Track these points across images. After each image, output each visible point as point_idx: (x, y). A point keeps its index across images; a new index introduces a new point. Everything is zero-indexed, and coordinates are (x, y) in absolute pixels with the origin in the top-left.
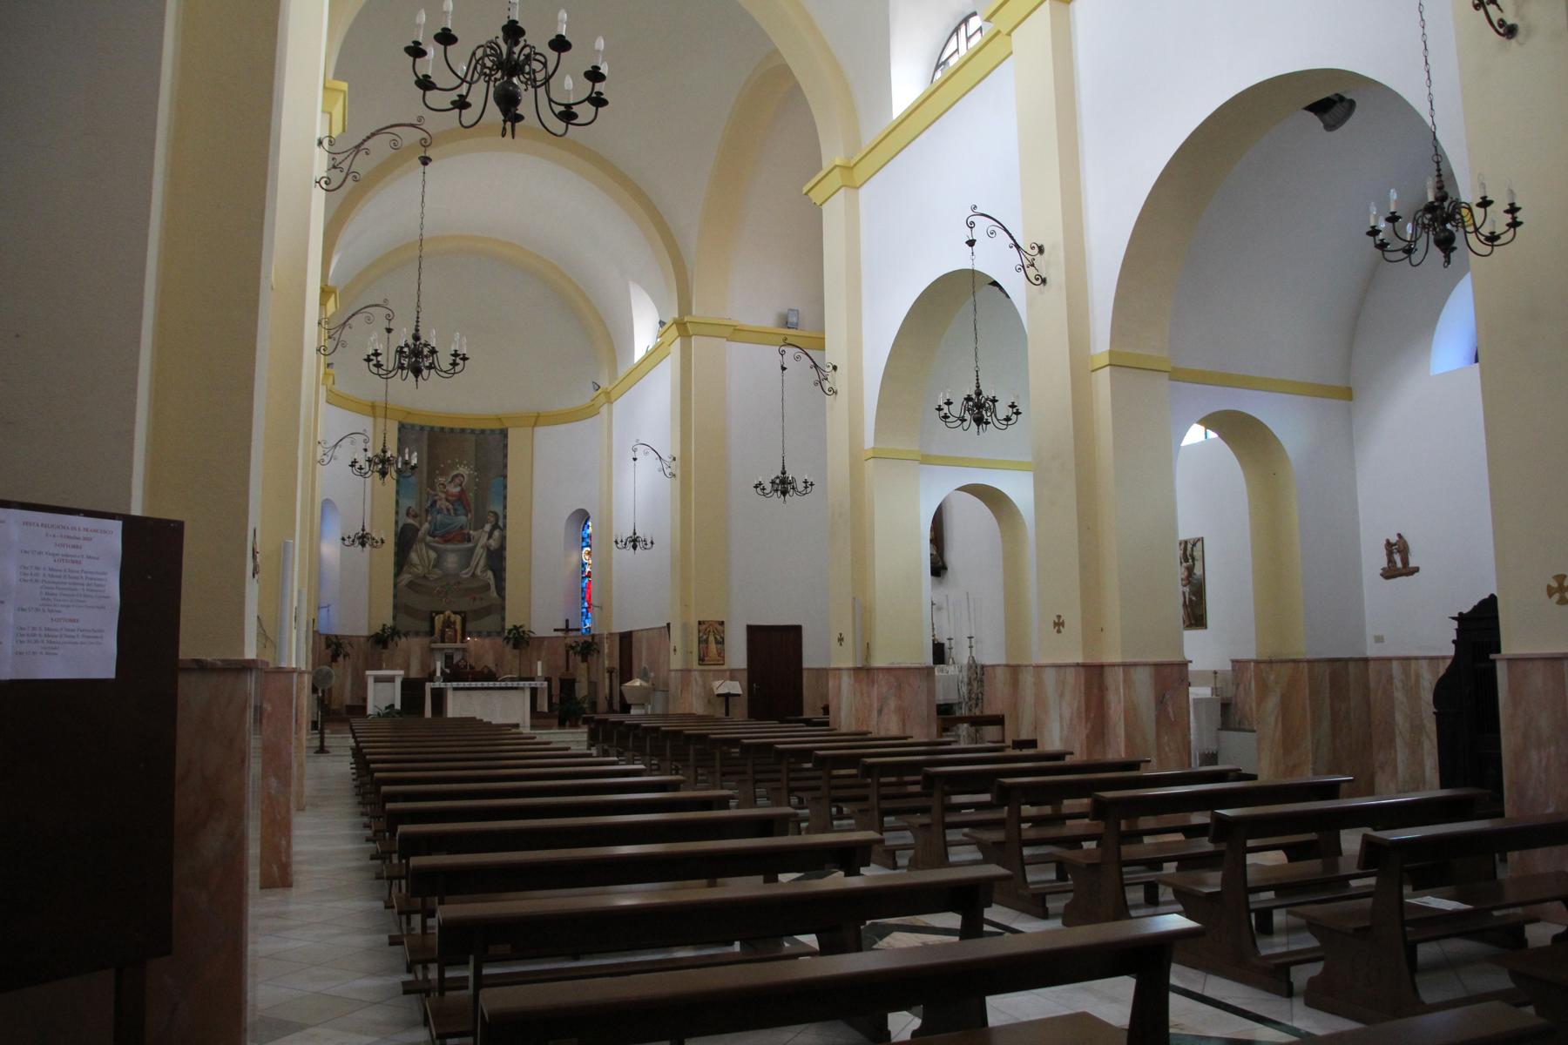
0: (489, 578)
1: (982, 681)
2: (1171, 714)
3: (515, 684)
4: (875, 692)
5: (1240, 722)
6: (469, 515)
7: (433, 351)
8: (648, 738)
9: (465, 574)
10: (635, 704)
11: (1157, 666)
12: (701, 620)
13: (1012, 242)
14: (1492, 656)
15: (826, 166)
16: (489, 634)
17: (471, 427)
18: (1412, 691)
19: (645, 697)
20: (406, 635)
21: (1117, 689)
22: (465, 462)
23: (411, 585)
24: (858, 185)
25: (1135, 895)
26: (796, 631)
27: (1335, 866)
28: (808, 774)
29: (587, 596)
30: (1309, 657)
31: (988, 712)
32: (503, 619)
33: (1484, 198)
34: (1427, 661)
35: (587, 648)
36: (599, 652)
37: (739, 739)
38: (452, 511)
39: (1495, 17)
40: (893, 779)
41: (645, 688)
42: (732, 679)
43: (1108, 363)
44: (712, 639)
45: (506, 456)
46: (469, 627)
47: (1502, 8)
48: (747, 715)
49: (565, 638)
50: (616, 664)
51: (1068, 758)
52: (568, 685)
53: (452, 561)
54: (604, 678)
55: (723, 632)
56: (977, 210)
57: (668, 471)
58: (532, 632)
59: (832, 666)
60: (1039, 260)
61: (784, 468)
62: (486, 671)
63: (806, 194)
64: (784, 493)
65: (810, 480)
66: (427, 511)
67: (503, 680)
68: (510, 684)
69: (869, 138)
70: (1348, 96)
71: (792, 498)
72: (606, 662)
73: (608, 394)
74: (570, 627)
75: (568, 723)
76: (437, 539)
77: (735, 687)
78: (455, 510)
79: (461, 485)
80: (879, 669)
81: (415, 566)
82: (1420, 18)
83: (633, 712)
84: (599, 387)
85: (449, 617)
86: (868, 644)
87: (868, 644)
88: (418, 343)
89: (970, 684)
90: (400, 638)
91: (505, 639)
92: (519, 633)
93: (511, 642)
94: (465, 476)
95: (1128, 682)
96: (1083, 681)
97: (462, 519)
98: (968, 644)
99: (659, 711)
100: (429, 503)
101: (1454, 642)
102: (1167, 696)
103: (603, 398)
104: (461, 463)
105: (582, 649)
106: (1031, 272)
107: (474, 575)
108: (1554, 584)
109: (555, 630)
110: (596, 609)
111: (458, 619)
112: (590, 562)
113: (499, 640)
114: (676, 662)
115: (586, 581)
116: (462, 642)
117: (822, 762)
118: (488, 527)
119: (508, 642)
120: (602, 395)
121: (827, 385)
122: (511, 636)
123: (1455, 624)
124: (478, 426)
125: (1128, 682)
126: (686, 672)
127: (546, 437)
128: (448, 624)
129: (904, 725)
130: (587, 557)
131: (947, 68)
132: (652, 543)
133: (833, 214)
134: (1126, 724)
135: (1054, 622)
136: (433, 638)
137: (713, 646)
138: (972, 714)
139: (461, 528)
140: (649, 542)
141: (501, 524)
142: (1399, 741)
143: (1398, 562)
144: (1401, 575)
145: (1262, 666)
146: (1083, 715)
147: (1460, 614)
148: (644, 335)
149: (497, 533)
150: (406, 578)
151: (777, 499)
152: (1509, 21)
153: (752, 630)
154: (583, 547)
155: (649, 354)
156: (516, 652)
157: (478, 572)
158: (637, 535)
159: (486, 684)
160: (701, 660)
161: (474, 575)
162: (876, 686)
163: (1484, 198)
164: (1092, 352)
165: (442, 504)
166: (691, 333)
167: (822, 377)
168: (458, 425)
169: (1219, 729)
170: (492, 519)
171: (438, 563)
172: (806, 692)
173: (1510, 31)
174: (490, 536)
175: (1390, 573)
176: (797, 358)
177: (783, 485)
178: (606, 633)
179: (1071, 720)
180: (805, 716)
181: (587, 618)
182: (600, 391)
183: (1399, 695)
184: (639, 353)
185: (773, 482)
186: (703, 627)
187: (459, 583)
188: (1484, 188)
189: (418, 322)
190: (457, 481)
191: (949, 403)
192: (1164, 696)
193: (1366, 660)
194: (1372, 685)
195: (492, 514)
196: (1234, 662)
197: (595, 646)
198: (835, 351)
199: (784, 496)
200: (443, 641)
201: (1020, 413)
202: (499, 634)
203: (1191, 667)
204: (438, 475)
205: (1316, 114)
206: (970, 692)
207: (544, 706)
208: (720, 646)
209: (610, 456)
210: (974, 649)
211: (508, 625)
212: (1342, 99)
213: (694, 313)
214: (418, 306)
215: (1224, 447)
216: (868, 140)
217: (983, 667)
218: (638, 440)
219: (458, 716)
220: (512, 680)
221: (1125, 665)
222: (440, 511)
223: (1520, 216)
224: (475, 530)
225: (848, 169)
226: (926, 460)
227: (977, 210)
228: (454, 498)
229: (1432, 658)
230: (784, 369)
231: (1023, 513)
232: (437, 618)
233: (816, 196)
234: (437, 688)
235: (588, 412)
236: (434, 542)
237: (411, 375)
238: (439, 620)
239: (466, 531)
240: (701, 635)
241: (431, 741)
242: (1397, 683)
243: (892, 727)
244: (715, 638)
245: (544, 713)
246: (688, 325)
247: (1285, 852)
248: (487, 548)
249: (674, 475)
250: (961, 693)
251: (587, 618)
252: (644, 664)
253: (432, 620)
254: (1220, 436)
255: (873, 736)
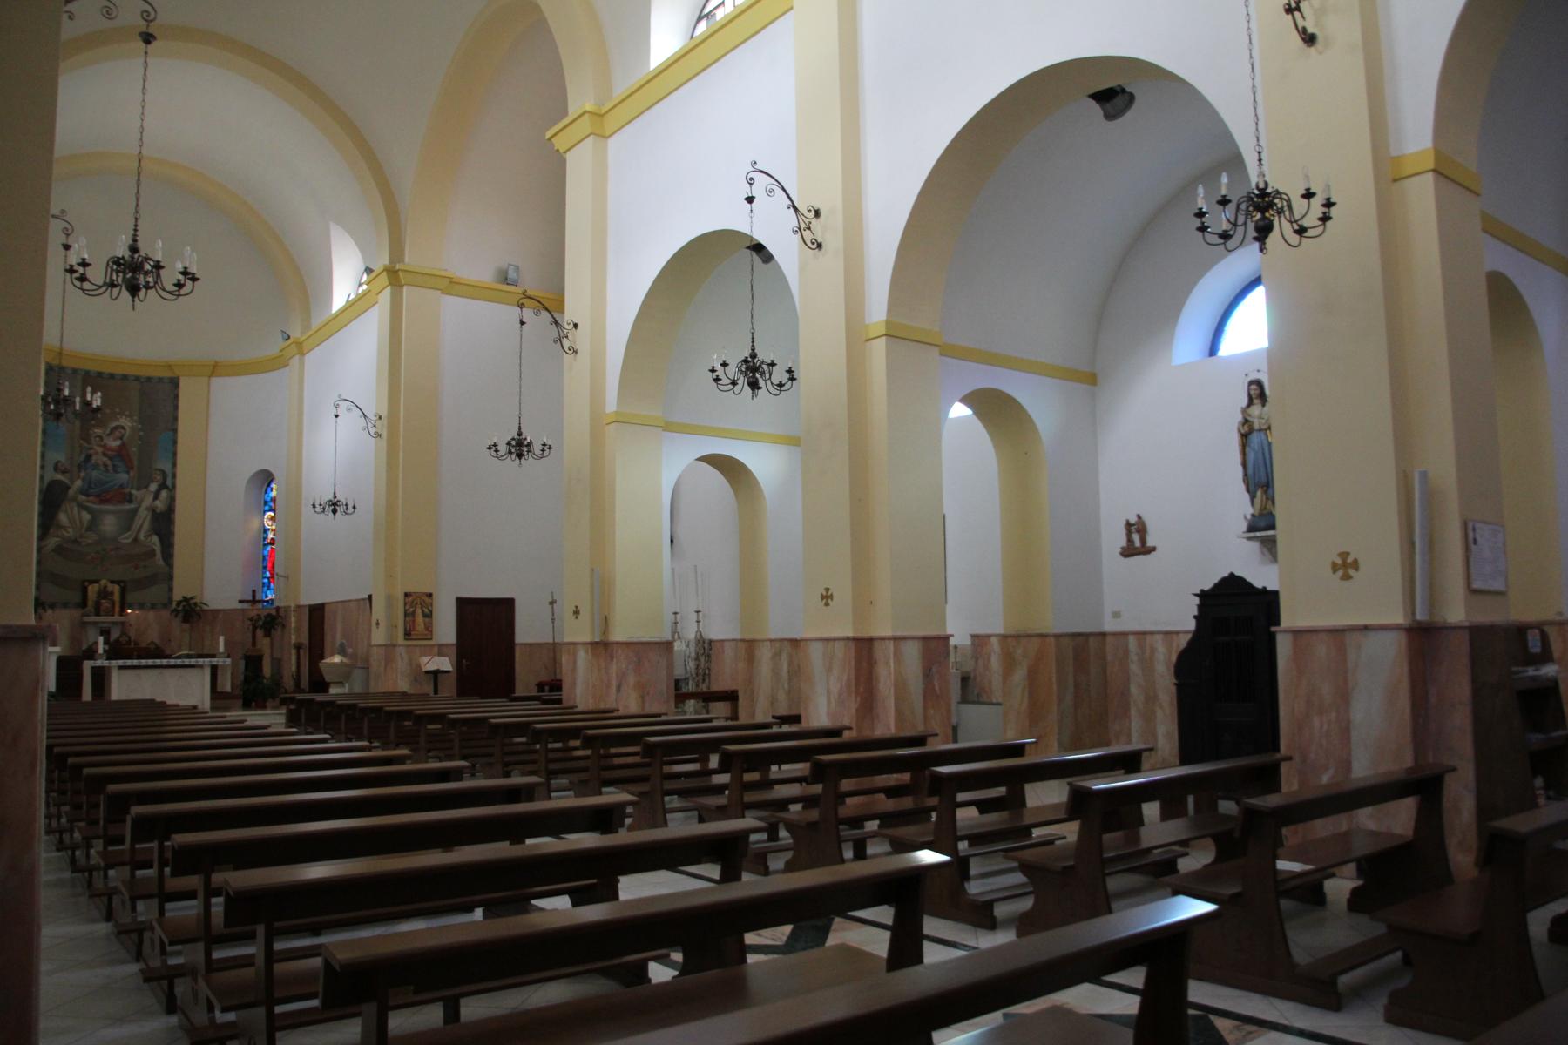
0: (154, 544)
1: (709, 656)
2: (937, 688)
3: (193, 661)
4: (614, 669)
5: (978, 695)
6: (132, 473)
7: (158, 266)
8: (366, 719)
9: (126, 539)
10: (334, 683)
11: (925, 639)
12: (408, 590)
13: (790, 203)
14: (1273, 629)
15: (573, 110)
16: (153, 606)
17: (148, 374)
18: (1147, 664)
19: (345, 674)
20: (53, 606)
21: (887, 663)
22: (127, 413)
23: (59, 550)
24: (608, 134)
25: (848, 854)
26: (508, 604)
27: (1136, 839)
28: (521, 748)
29: (269, 565)
30: (1056, 631)
31: (715, 687)
32: (171, 590)
33: (1308, 190)
34: (1161, 635)
35: (271, 622)
36: (284, 626)
37: (486, 719)
38: (110, 468)
39: (1301, 23)
40: (558, 745)
41: (346, 665)
42: (440, 654)
43: (884, 332)
44: (419, 611)
45: (176, 407)
46: (130, 598)
47: (1305, 15)
48: (455, 691)
49: (253, 610)
50: (305, 639)
51: (846, 734)
52: (253, 662)
53: (109, 524)
54: (291, 654)
55: (431, 605)
56: (756, 167)
57: (372, 431)
58: (206, 605)
59: (567, 639)
60: (815, 223)
61: (520, 429)
62: (152, 647)
63: (550, 139)
64: (520, 456)
65: (548, 443)
66: (79, 467)
67: (177, 658)
68: (187, 662)
69: (620, 88)
70: (1129, 89)
71: (528, 461)
72: (293, 637)
73: (299, 344)
74: (251, 598)
75: (253, 704)
76: (91, 498)
77: (445, 664)
78: (114, 466)
79: (121, 438)
80: (618, 643)
81: (64, 528)
82: (1245, 12)
83: (333, 690)
84: (289, 337)
85: (105, 587)
86: (606, 617)
87: (606, 617)
88: (136, 256)
89: (697, 659)
90: (45, 611)
91: (173, 611)
92: (189, 605)
93: (181, 615)
94: (128, 430)
95: (898, 654)
96: (853, 655)
97: (123, 477)
98: (695, 619)
99: (358, 689)
100: (83, 457)
101: (1195, 617)
102: (934, 669)
103: (294, 348)
104: (122, 414)
105: (264, 623)
106: (807, 234)
107: (136, 540)
108: (1339, 561)
109: (240, 602)
110: (282, 579)
111: (116, 589)
112: (274, 527)
113: (166, 614)
114: (379, 637)
115: (269, 548)
116: (121, 615)
117: (538, 736)
118: (153, 487)
119: (176, 616)
120: (293, 346)
121: (566, 343)
122: (180, 608)
123: (1197, 601)
124: (144, 373)
125: (898, 654)
126: (390, 647)
127: (228, 394)
128: (104, 594)
129: (643, 702)
130: (270, 523)
131: (711, 21)
132: (354, 507)
133: (579, 165)
134: (897, 699)
135: (822, 595)
136: (86, 610)
137: (420, 619)
138: (699, 690)
139: (122, 486)
140: (350, 507)
141: (169, 483)
142: (1133, 712)
143: (1137, 542)
144: (1139, 554)
145: (1010, 640)
146: (853, 688)
147: (1202, 591)
148: (344, 285)
149: (164, 494)
150: (52, 542)
151: (511, 463)
152: (1310, 30)
153: (463, 604)
154: (265, 512)
155: (350, 305)
156: (186, 626)
157: (142, 536)
158: (338, 498)
159: (150, 662)
160: (408, 634)
161: (136, 540)
162: (615, 660)
163: (1308, 190)
164: (867, 322)
165: (99, 458)
166: (403, 282)
167: (562, 334)
168: (118, 371)
169: (959, 703)
170: (159, 478)
171: (93, 526)
172: (518, 667)
173: (1309, 39)
174: (156, 497)
175: (1129, 552)
176: (537, 313)
177: (519, 447)
178: (293, 605)
179: (840, 695)
180: (516, 695)
181: (269, 588)
182: (290, 341)
183: (1134, 668)
184: (338, 302)
185: (509, 443)
186: (410, 599)
187: (118, 548)
188: (1308, 180)
189: (136, 230)
190: (117, 433)
191: (724, 364)
192: (930, 670)
193: (1104, 635)
194: (1109, 658)
195: (158, 472)
196: (974, 637)
197: (280, 620)
198: (575, 307)
199: (520, 459)
200: (98, 614)
201: (1334, 204)
202: (165, 606)
203: (952, 642)
204: (94, 426)
205: (1098, 103)
206: (697, 667)
207: (226, 685)
208: (427, 620)
209: (300, 414)
210: (701, 624)
211: (177, 596)
212: (1123, 91)
213: (407, 260)
214: (137, 212)
215: (978, 426)
216: (620, 90)
217: (711, 642)
218: (340, 395)
219: (124, 698)
220: (189, 656)
221: (895, 639)
222: (96, 467)
223: (1334, 211)
224: (138, 489)
225: (598, 116)
226: (669, 427)
227: (756, 167)
228: (114, 453)
229: (1167, 633)
230: (522, 323)
231: (762, 485)
232: (90, 588)
233: (560, 143)
234: (100, 667)
235: (277, 363)
236: (88, 502)
237: (125, 294)
238: (93, 590)
239: (127, 491)
240: (407, 607)
241: (99, 736)
242: (1133, 657)
243: (630, 704)
244: (423, 611)
245: (227, 693)
246: (400, 274)
247: (978, 808)
248: (153, 510)
249: (380, 435)
250: (688, 668)
251: (269, 588)
252: (338, 641)
253: (85, 591)
254: (976, 413)
255: (621, 713)
